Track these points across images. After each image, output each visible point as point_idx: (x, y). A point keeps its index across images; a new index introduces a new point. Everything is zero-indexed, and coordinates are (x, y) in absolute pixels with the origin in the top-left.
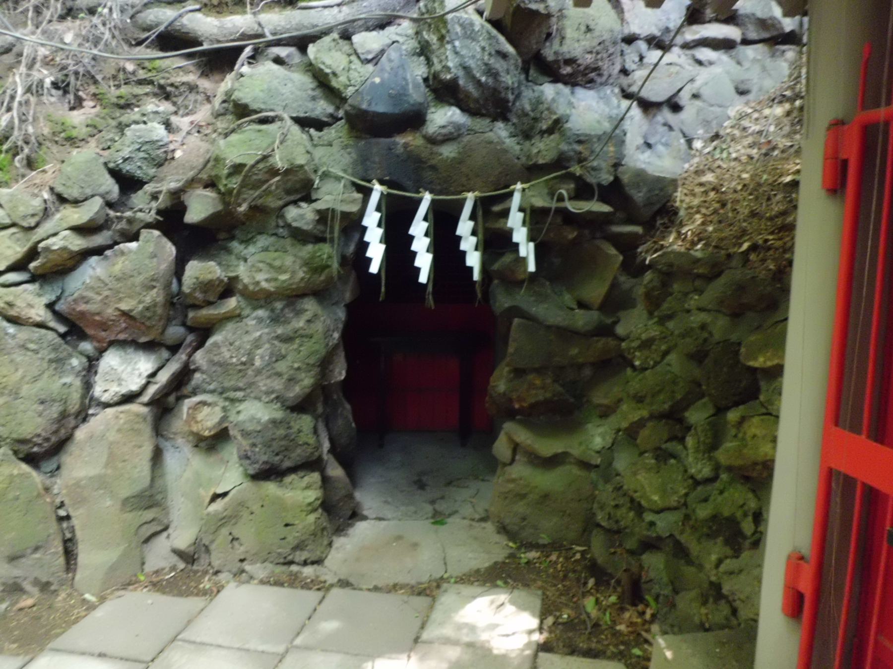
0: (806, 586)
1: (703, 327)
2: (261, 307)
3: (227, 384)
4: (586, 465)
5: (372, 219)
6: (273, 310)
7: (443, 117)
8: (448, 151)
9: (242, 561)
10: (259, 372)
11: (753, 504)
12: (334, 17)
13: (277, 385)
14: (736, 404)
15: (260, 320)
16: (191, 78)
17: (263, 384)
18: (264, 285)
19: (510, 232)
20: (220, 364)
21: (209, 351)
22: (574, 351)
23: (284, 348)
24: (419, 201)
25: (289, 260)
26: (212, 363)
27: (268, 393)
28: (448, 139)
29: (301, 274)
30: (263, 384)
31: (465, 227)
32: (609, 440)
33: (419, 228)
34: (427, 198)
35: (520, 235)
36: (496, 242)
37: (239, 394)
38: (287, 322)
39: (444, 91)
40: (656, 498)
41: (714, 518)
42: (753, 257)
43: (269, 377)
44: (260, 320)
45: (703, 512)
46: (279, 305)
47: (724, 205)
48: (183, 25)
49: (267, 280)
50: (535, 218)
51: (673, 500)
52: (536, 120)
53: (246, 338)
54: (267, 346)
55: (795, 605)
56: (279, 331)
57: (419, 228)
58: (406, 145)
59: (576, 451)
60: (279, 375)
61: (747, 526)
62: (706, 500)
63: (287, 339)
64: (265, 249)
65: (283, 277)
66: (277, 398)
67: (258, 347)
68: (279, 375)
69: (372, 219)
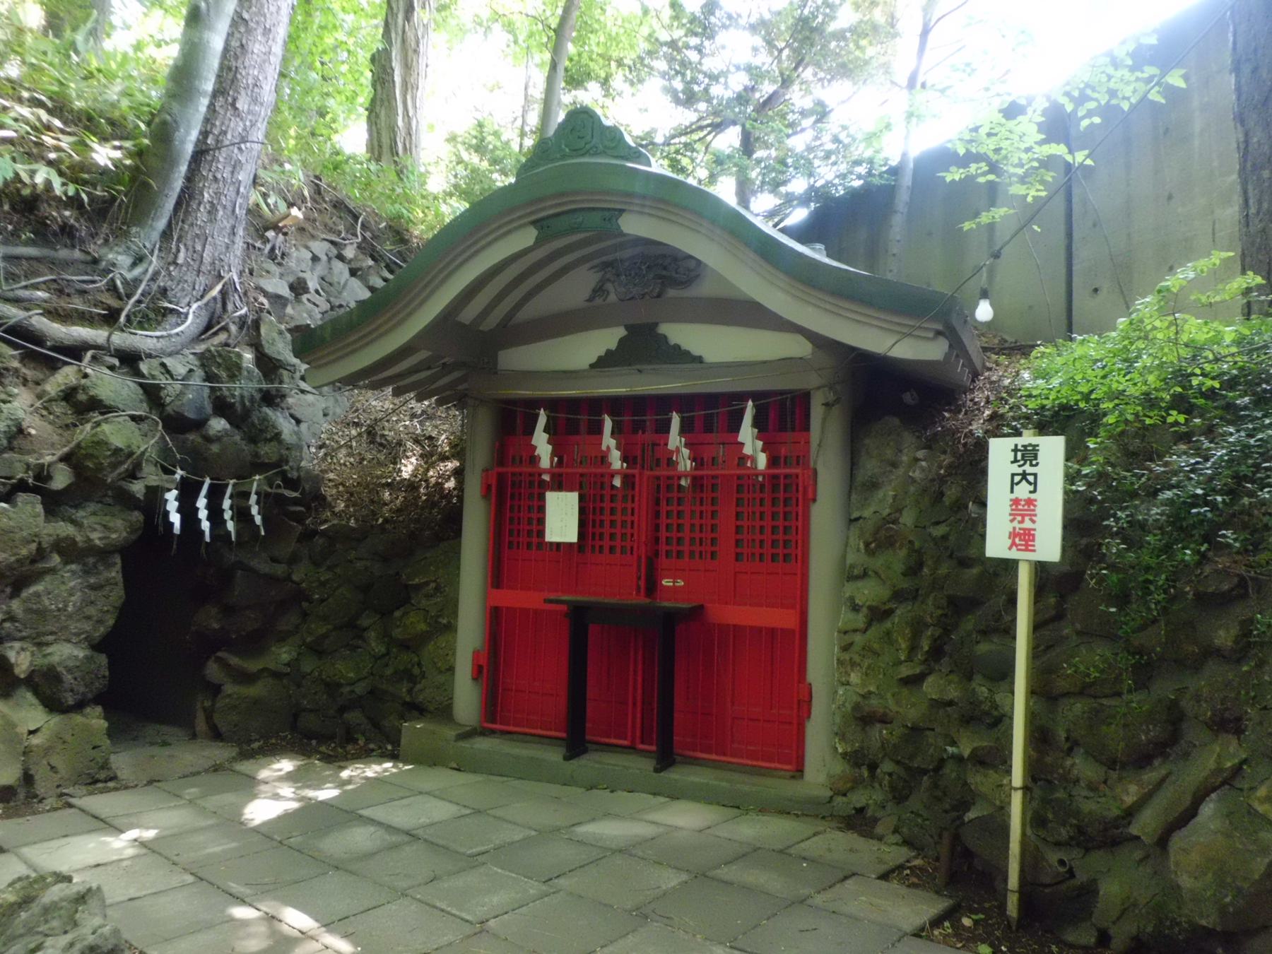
0: (483, 661)
1: (366, 568)
2: (72, 562)
3: (42, 629)
4: (276, 675)
5: (171, 496)
6: (84, 565)
7: (218, 425)
8: (215, 448)
9: (58, 786)
10: (70, 617)
11: (416, 659)
12: (151, 346)
13: (87, 626)
14: (398, 608)
15: (74, 573)
16: (16, 364)
17: (74, 627)
18: (97, 542)
19: (249, 508)
20: (36, 612)
21: (28, 600)
22: (273, 593)
23: (93, 595)
24: (203, 483)
25: (119, 523)
26: (28, 611)
27: (77, 635)
28: (218, 439)
29: (125, 534)
30: (74, 627)
31: (227, 503)
32: (294, 654)
33: (202, 503)
34: (208, 481)
35: (254, 510)
36: (242, 515)
37: (51, 638)
38: (99, 573)
39: (222, 407)
40: (351, 675)
41: (396, 672)
42: (387, 526)
43: (79, 620)
44: (74, 573)
45: (389, 671)
46: (91, 560)
47: (352, 495)
48: (32, 325)
49: (100, 539)
50: (263, 498)
51: (365, 673)
52: (261, 431)
53: (63, 588)
54: (79, 594)
55: (478, 672)
56: (92, 581)
57: (202, 503)
58: (193, 441)
59: (272, 666)
60: (88, 618)
61: (416, 671)
62: (387, 665)
63: (93, 588)
64: (94, 514)
65: (114, 536)
66: (86, 638)
67: (71, 595)
68: (88, 618)
69: (171, 496)
